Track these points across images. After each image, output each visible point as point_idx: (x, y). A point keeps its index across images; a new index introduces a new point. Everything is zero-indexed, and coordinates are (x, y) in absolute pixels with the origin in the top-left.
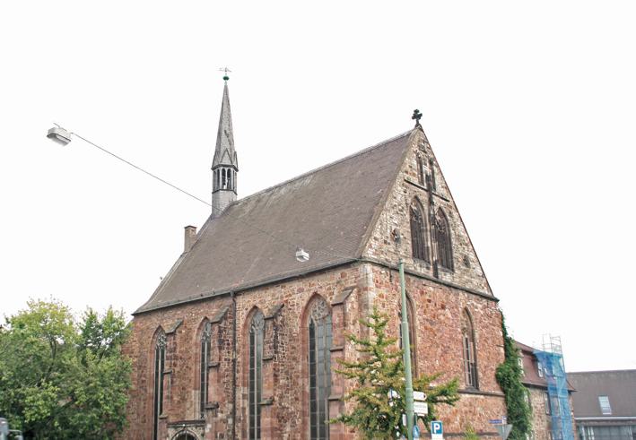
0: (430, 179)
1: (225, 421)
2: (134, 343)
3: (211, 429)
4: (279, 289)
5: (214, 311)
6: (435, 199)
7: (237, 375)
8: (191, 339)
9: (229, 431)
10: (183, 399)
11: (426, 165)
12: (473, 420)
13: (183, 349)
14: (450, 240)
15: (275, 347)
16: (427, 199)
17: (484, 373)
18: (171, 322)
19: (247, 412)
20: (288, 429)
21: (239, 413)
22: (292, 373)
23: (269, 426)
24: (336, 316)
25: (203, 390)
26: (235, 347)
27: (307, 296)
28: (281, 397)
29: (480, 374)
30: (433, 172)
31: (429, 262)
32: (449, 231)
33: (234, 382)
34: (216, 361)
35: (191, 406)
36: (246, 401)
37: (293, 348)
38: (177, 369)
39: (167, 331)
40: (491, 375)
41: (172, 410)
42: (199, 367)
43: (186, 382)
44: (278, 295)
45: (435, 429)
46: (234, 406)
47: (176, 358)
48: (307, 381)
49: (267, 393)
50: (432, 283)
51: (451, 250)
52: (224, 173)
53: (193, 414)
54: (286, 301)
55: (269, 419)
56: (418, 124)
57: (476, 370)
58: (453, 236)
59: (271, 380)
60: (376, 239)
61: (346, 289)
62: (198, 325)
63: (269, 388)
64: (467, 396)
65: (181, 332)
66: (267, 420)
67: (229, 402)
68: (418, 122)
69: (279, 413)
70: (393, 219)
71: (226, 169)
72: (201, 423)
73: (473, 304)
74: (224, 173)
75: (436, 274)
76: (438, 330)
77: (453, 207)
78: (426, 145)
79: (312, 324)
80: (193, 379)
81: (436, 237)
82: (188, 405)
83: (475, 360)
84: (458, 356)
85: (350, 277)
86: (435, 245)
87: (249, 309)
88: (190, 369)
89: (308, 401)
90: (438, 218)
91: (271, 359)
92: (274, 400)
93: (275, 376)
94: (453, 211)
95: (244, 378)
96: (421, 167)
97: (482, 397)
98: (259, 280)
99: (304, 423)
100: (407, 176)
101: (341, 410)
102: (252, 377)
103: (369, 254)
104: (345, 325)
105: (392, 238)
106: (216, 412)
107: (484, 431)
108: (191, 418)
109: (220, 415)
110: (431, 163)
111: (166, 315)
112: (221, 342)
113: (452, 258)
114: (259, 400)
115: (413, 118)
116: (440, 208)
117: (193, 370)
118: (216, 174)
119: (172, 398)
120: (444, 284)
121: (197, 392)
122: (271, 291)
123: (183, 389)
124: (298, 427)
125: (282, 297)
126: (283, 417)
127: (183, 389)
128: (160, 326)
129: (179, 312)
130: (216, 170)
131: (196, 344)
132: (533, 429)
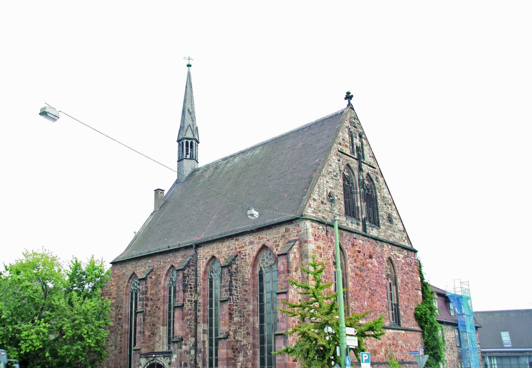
0: (360, 150)
1: (189, 353)
2: (112, 287)
3: (176, 359)
4: (233, 241)
5: (179, 260)
6: (364, 167)
7: (198, 314)
8: (160, 283)
9: (191, 360)
10: (153, 334)
11: (356, 138)
12: (396, 351)
13: (153, 292)
15: (230, 290)
16: (357, 166)
17: (405, 312)
18: (143, 269)
20: (241, 359)
21: (200, 346)
25: (169, 326)
26: (196, 290)
28: (235, 332)
29: (402, 313)
30: (362, 144)
31: (359, 219)
33: (196, 320)
35: (160, 339)
36: (206, 335)
37: (245, 291)
38: (148, 309)
39: (140, 277)
42: (167, 307)
44: (233, 247)
45: (364, 358)
47: (147, 299)
48: (257, 319)
49: (223, 329)
50: (361, 237)
54: (240, 252)
56: (349, 104)
59: (227, 317)
60: (314, 200)
62: (165, 272)
63: (225, 325)
64: (391, 331)
65: (151, 278)
66: (223, 352)
67: (191, 337)
68: (349, 102)
69: (233, 346)
70: (329, 183)
71: (189, 142)
73: (395, 254)
75: (365, 229)
76: (367, 276)
77: (379, 173)
78: (356, 122)
79: (261, 271)
81: (364, 198)
82: (157, 339)
84: (384, 298)
86: (364, 205)
87: (209, 258)
88: (159, 308)
89: (258, 335)
90: (366, 182)
91: (227, 300)
92: (229, 335)
93: (230, 314)
94: (379, 176)
95: (204, 316)
96: (352, 140)
97: (403, 332)
99: (254, 353)
100: (340, 147)
101: (285, 343)
102: (211, 315)
103: (309, 212)
104: (289, 272)
105: (328, 200)
107: (405, 361)
108: (160, 350)
109: (184, 347)
110: (360, 137)
111: (139, 264)
112: (185, 286)
114: (217, 334)
115: (346, 98)
117: (162, 309)
119: (144, 332)
121: (165, 327)
122: (227, 243)
123: (154, 325)
124: (249, 357)
125: (236, 249)
126: (237, 349)
127: (154, 325)
128: (134, 273)
129: (150, 261)
130: (181, 143)
131: (164, 288)
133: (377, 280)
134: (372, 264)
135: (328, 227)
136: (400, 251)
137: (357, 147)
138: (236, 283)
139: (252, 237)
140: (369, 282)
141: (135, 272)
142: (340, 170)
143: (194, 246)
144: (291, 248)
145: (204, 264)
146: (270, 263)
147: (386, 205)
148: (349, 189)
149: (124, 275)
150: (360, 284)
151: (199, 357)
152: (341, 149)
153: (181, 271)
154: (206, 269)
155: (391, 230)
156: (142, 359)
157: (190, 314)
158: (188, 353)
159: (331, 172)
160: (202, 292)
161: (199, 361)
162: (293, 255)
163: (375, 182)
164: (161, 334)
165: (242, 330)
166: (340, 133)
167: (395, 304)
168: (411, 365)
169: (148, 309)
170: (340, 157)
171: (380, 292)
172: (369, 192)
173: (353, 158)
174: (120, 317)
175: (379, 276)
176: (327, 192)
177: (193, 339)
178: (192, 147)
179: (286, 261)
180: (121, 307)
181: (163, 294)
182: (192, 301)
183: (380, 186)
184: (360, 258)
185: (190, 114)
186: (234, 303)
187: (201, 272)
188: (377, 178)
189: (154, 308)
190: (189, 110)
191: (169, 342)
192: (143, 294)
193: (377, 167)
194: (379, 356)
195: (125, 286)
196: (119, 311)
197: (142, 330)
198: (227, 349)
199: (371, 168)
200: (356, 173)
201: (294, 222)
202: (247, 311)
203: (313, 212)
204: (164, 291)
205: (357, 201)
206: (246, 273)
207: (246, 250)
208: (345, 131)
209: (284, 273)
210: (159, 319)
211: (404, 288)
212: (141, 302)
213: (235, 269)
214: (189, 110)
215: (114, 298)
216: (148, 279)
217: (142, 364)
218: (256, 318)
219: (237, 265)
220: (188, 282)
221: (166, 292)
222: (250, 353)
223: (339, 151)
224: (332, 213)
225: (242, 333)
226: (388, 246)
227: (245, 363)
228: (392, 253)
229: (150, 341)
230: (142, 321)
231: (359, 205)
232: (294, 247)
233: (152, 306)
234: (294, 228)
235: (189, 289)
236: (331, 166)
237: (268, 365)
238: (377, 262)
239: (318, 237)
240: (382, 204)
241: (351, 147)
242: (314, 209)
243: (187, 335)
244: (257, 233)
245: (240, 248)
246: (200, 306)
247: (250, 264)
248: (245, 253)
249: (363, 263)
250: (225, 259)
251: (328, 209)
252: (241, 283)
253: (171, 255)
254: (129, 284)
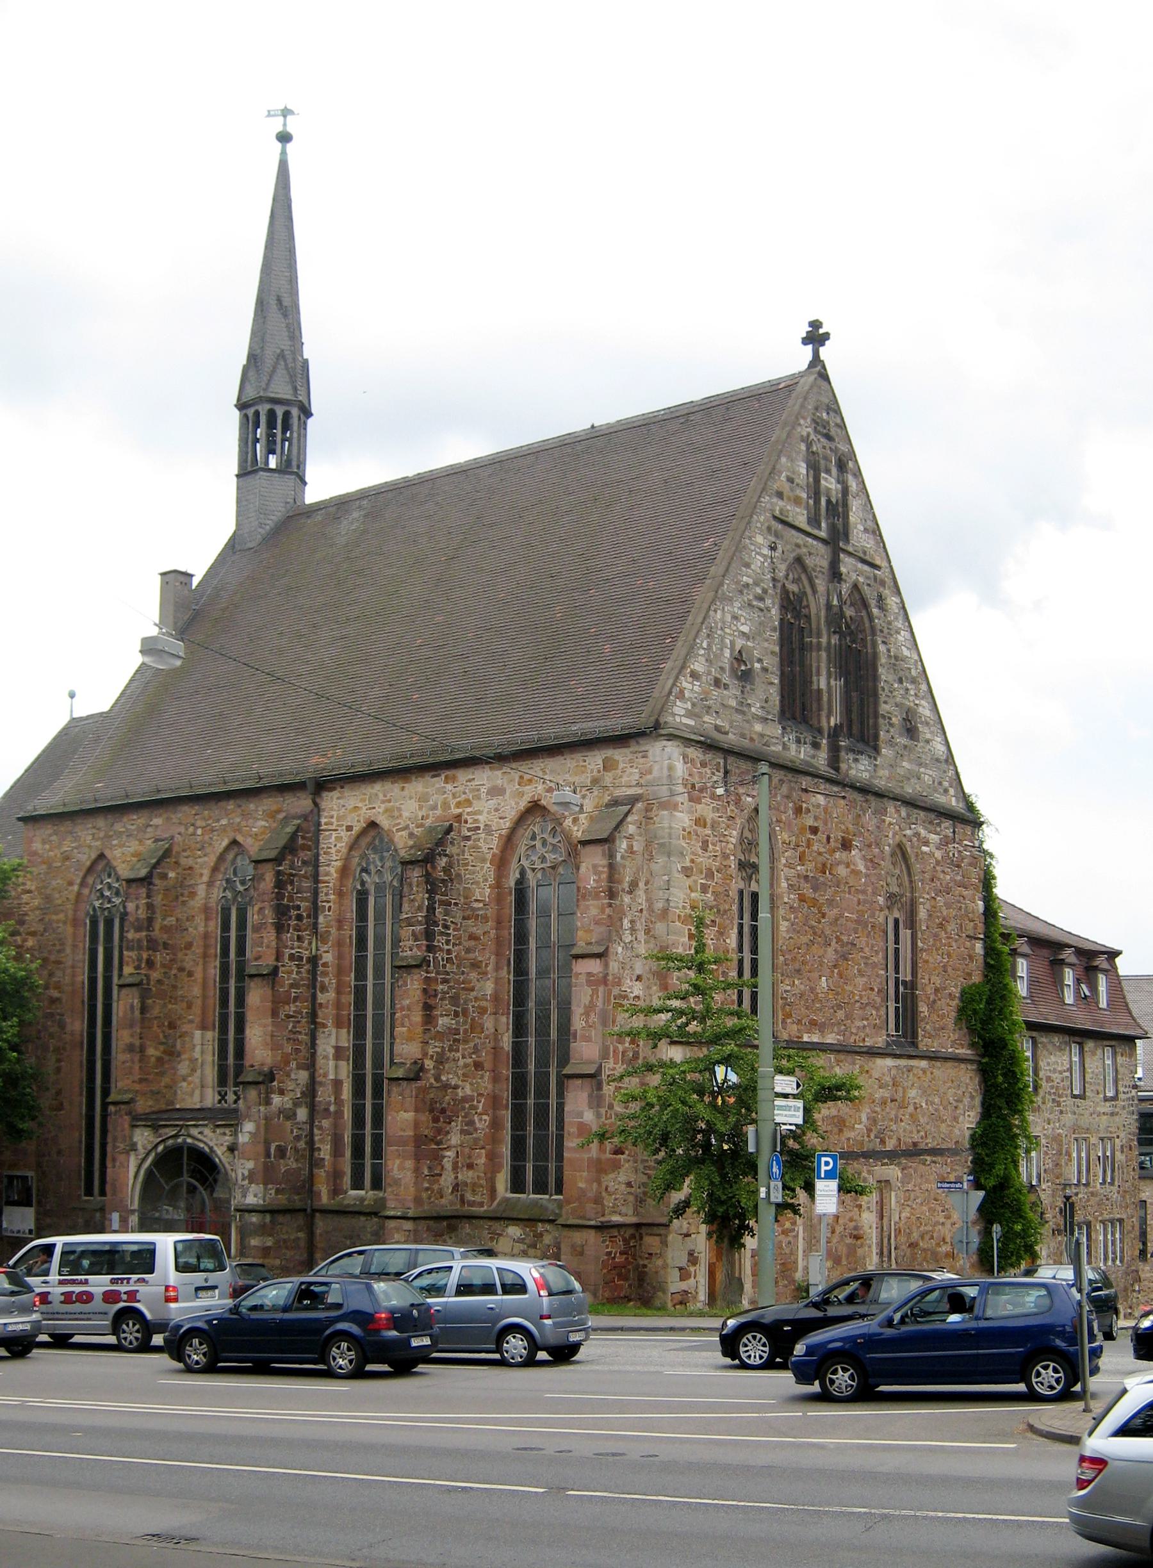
0: (838, 511)
1: (290, 1115)
2: (25, 897)
3: (253, 1135)
4: (438, 782)
5: (258, 826)
6: (847, 565)
7: (321, 998)
8: (193, 895)
9: (298, 1138)
10: (172, 1054)
11: (828, 472)
12: (898, 1120)
13: (171, 921)
14: (875, 669)
15: (429, 935)
16: (825, 564)
17: (932, 1005)
18: (134, 846)
19: (346, 1093)
20: (455, 1139)
21: (324, 1095)
22: (466, 1001)
23: (412, 1133)
24: (592, 863)
25: (224, 1030)
27: (512, 807)
28: (440, 1060)
29: (923, 1008)
30: (845, 491)
32: (874, 645)
33: (313, 1015)
34: (269, 961)
35: (194, 1070)
36: (343, 1064)
37: (472, 937)
38: (155, 975)
39: (124, 871)
40: (949, 1008)
41: (141, 1081)
42: (214, 971)
43: (179, 1008)
45: (824, 1168)
46: (312, 1077)
47: (152, 944)
48: (506, 1022)
49: (407, 1049)
50: (823, 786)
51: (876, 695)
52: (274, 415)
53: (197, 1085)
54: (458, 817)
55: (409, 1116)
56: (816, 361)
57: (914, 998)
58: (883, 660)
59: (417, 1017)
60: (695, 675)
61: (615, 803)
62: (211, 860)
63: (410, 1039)
64: (889, 1062)
65: (164, 876)
66: (401, 1118)
67: (298, 1068)
68: (816, 354)
69: (433, 1102)
70: (742, 625)
71: (280, 411)
72: (227, 1118)
73: (917, 834)
74: (274, 415)
75: (834, 761)
76: (831, 902)
77: (889, 582)
78: (833, 419)
79: (521, 884)
80: (199, 1002)
81: (841, 667)
82: (183, 1068)
83: (914, 973)
84: (874, 965)
85: (629, 771)
86: (837, 684)
87: (357, 829)
88: (190, 974)
89: (507, 1072)
90: (849, 612)
92: (422, 1069)
93: (428, 1008)
94: (886, 592)
95: (338, 1005)
96: (817, 480)
97: (924, 1064)
98: (382, 755)
99: (495, 1124)
101: (596, 1101)
102: (360, 1002)
103: (679, 715)
104: (612, 894)
105: (734, 671)
106: (268, 1093)
107: (922, 1146)
108: (194, 1102)
109: (276, 1099)
110: (842, 466)
111: (119, 827)
112: (281, 911)
113: (876, 715)
114: (378, 1063)
115: (806, 341)
116: (855, 586)
117: (198, 975)
118: (249, 423)
119: (142, 1049)
120: (853, 787)
121: (209, 1035)
122: (418, 786)
124: (479, 1134)
126: (443, 1111)
127: (172, 1026)
128: (101, 856)
129: (157, 821)
130: (250, 412)
131: (206, 909)
132: (1035, 1131)
133: (861, 913)
134: (848, 865)
135: (731, 759)
136: (931, 823)
137: (829, 502)
138: (447, 913)
139: (499, 773)
140: (837, 920)
141: (107, 853)
142: (774, 579)
143: (311, 786)
144: (622, 821)
145: (343, 846)
146: (551, 857)
147: (900, 681)
148: (795, 638)
149: (67, 858)
150: (812, 927)
151: (320, 1128)
152: (781, 511)
153: (269, 866)
154: (347, 859)
155: (910, 761)
156: (138, 1131)
157: (296, 999)
158: (287, 1118)
159: (747, 585)
160: (333, 931)
161: (322, 1141)
162: (624, 845)
163: (875, 611)
164: (197, 1054)
165: (459, 1055)
166: (783, 460)
167: (905, 983)
168: (939, 1159)
169: (155, 975)
170: (777, 535)
171: (866, 949)
172: (853, 641)
173: (815, 537)
174: (55, 994)
175: (865, 901)
176: (732, 649)
177: (303, 1076)
178: (286, 427)
179: (605, 862)
180: (59, 962)
181: (201, 929)
182: (301, 959)
183: (890, 623)
184: (815, 848)
185: (285, 316)
186: (438, 973)
187: (333, 870)
188: (880, 598)
189: (174, 972)
190: (279, 301)
191: (222, 1080)
192: (138, 929)
193: (884, 564)
194: (852, 1135)
195: (72, 897)
196: (51, 975)
197: (137, 1043)
198: (417, 1110)
199: (866, 568)
200: (821, 584)
201: (633, 742)
202: (476, 999)
203: (689, 714)
204: (207, 919)
205: (818, 674)
206: (477, 883)
207: (479, 812)
208: (798, 453)
209: (597, 896)
210: (189, 1007)
211: (936, 935)
212: (133, 954)
213: (445, 870)
214: (279, 301)
215: (33, 934)
216: (156, 881)
217: (140, 1147)
218: (504, 1019)
219: (450, 856)
220: (291, 899)
221: (212, 924)
222: (482, 1123)
223: (775, 517)
224: (744, 713)
225: (461, 1062)
226: (898, 811)
227: (467, 1150)
228: (908, 832)
229: (162, 1074)
230: (137, 1013)
231: (823, 685)
232: (629, 819)
233: (167, 966)
234: (631, 761)
235: (293, 923)
236: (748, 565)
237: (536, 1159)
238: (864, 858)
239: (701, 790)
240: (891, 678)
241: (811, 502)
242: (693, 705)
243: (287, 1063)
244: (514, 765)
245: (458, 805)
246: (325, 974)
247: (489, 856)
248: (476, 821)
249: (824, 865)
250: (411, 835)
251: (733, 703)
252: (460, 914)
253: (231, 805)
254: (86, 891)
